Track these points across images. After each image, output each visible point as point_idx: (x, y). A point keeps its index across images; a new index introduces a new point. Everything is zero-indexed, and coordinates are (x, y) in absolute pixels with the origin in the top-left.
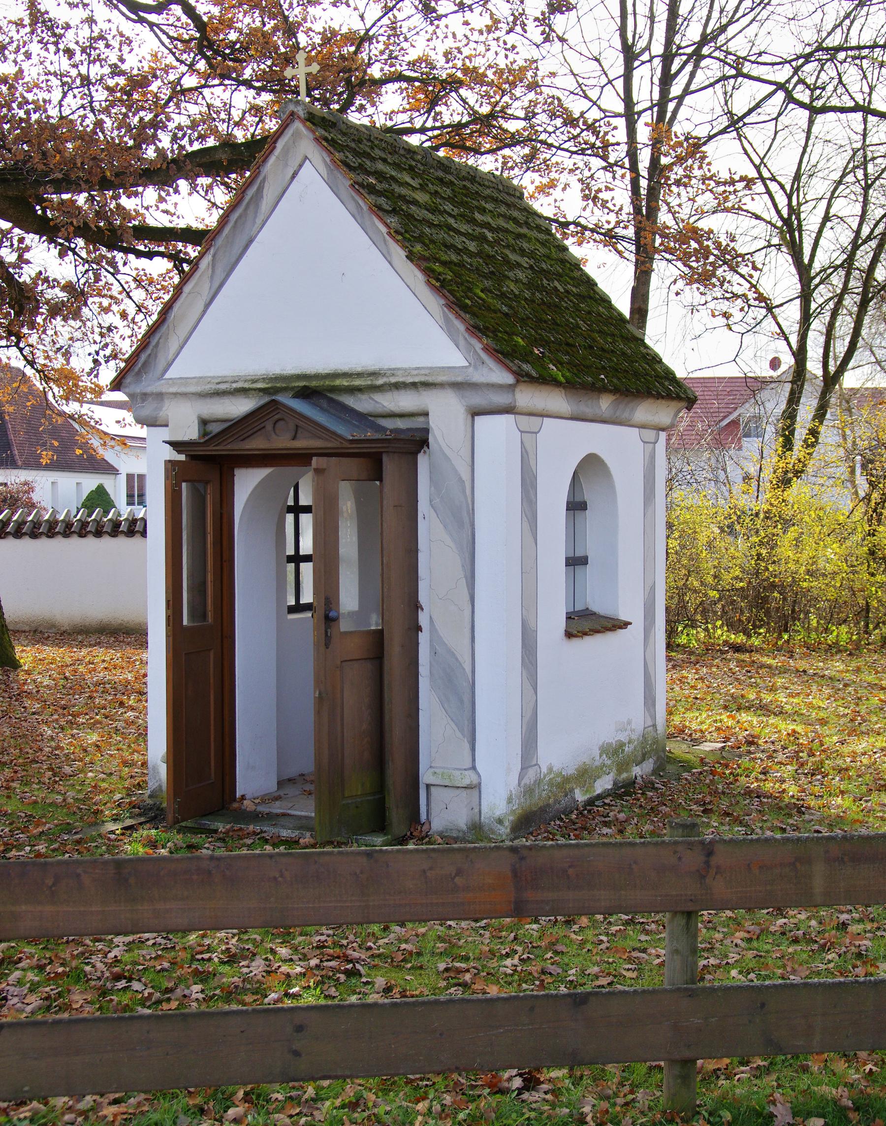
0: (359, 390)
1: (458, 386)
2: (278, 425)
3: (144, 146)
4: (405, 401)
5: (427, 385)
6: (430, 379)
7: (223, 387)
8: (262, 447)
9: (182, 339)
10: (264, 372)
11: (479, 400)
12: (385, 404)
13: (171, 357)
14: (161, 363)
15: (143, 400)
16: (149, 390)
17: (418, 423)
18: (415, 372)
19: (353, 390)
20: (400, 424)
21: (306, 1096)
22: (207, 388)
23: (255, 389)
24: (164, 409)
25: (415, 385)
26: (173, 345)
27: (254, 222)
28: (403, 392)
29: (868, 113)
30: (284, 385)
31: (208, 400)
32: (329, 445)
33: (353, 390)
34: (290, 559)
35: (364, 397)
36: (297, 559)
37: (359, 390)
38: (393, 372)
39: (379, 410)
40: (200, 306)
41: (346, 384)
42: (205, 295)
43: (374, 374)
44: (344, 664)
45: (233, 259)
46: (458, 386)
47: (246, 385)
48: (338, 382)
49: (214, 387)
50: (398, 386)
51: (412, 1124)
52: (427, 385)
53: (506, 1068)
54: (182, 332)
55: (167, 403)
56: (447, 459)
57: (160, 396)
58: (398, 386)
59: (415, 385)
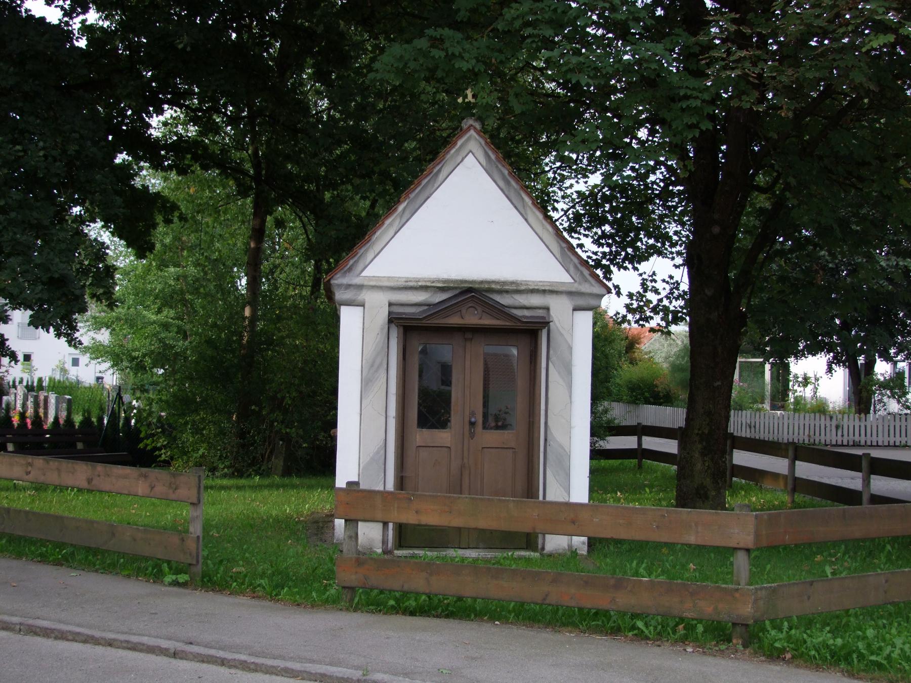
0: (507, 292)
1: (570, 294)
4: (535, 300)
5: (552, 292)
6: (555, 289)
7: (411, 284)
9: (376, 253)
11: (581, 302)
13: (367, 263)
14: (360, 266)
16: (350, 283)
17: (540, 313)
18: (541, 284)
19: (500, 292)
20: (526, 313)
22: (401, 283)
25: (544, 292)
26: (370, 256)
27: (433, 186)
29: (796, 458)
32: (507, 324)
33: (500, 292)
35: (507, 296)
37: (507, 292)
38: (526, 283)
39: (517, 304)
42: (395, 228)
44: (485, 450)
45: (417, 207)
46: (570, 294)
48: (493, 286)
49: (404, 284)
50: (533, 291)
51: (907, 190)
52: (552, 292)
54: (377, 248)
56: (562, 334)
57: (360, 287)
58: (533, 291)
59: (544, 292)
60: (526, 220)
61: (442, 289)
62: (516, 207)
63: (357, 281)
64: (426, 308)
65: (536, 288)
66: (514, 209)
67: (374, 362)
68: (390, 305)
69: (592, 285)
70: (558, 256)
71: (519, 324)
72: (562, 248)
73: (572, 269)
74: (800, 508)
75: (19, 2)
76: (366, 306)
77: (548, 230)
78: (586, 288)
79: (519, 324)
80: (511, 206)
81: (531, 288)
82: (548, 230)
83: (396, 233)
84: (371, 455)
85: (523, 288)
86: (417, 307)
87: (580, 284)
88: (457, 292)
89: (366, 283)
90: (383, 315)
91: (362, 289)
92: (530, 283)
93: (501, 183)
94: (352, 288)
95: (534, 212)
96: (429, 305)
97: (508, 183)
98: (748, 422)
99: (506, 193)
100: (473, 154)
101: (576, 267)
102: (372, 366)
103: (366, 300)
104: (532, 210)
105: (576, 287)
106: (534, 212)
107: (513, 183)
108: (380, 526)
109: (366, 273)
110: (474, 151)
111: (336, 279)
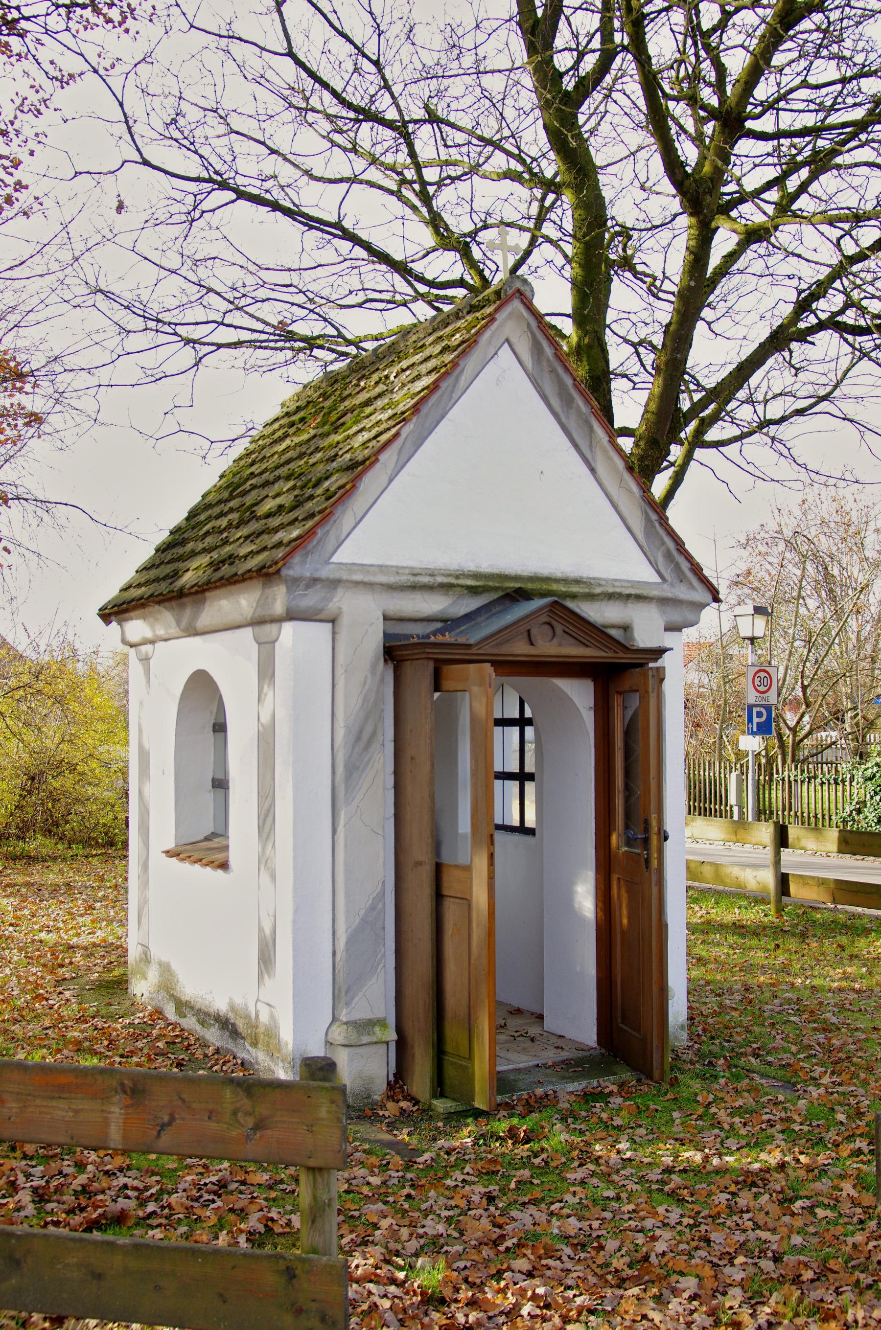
1: (663, 601)
2: (547, 627)
3: (693, 284)
5: (639, 598)
6: (645, 592)
7: (425, 580)
8: (525, 652)
10: (456, 568)
12: (591, 614)
15: (308, 587)
16: (317, 575)
19: (591, 597)
21: (481, 1315)
22: (404, 579)
23: (458, 586)
24: (335, 600)
28: (611, 603)
30: (497, 585)
31: (396, 594)
32: (605, 654)
33: (574, 596)
34: (531, 777)
36: (522, 777)
38: (597, 582)
40: (386, 479)
41: (564, 589)
43: (578, 581)
46: (663, 601)
47: (453, 581)
50: (611, 596)
52: (639, 598)
53: (347, 1295)
55: (340, 592)
57: (334, 584)
58: (611, 596)
60: (593, 470)
61: (473, 591)
62: (576, 446)
63: (325, 572)
64: (439, 625)
65: (618, 590)
66: (573, 451)
67: (361, 731)
68: (386, 618)
69: (693, 588)
70: (640, 536)
71: (621, 655)
72: (648, 519)
73: (661, 561)
74: (801, 876)
75: (3, 652)
76: (344, 622)
77: (630, 491)
78: (682, 592)
79: (621, 655)
80: (569, 444)
81: (611, 590)
82: (630, 491)
83: (391, 481)
84: (362, 913)
85: (598, 590)
86: (425, 623)
87: (672, 585)
88: (494, 596)
89: (345, 576)
90: (374, 641)
91: (335, 588)
92: (603, 583)
93: (556, 403)
94: (319, 586)
95: (609, 458)
96: (445, 621)
97: (568, 402)
98: (840, 788)
99: (564, 420)
100: (510, 346)
101: (668, 556)
102: (358, 738)
103: (345, 608)
104: (605, 451)
105: (668, 591)
106: (609, 458)
107: (579, 401)
108: (385, 1046)
109: (343, 556)
110: (513, 340)
111: (290, 568)
